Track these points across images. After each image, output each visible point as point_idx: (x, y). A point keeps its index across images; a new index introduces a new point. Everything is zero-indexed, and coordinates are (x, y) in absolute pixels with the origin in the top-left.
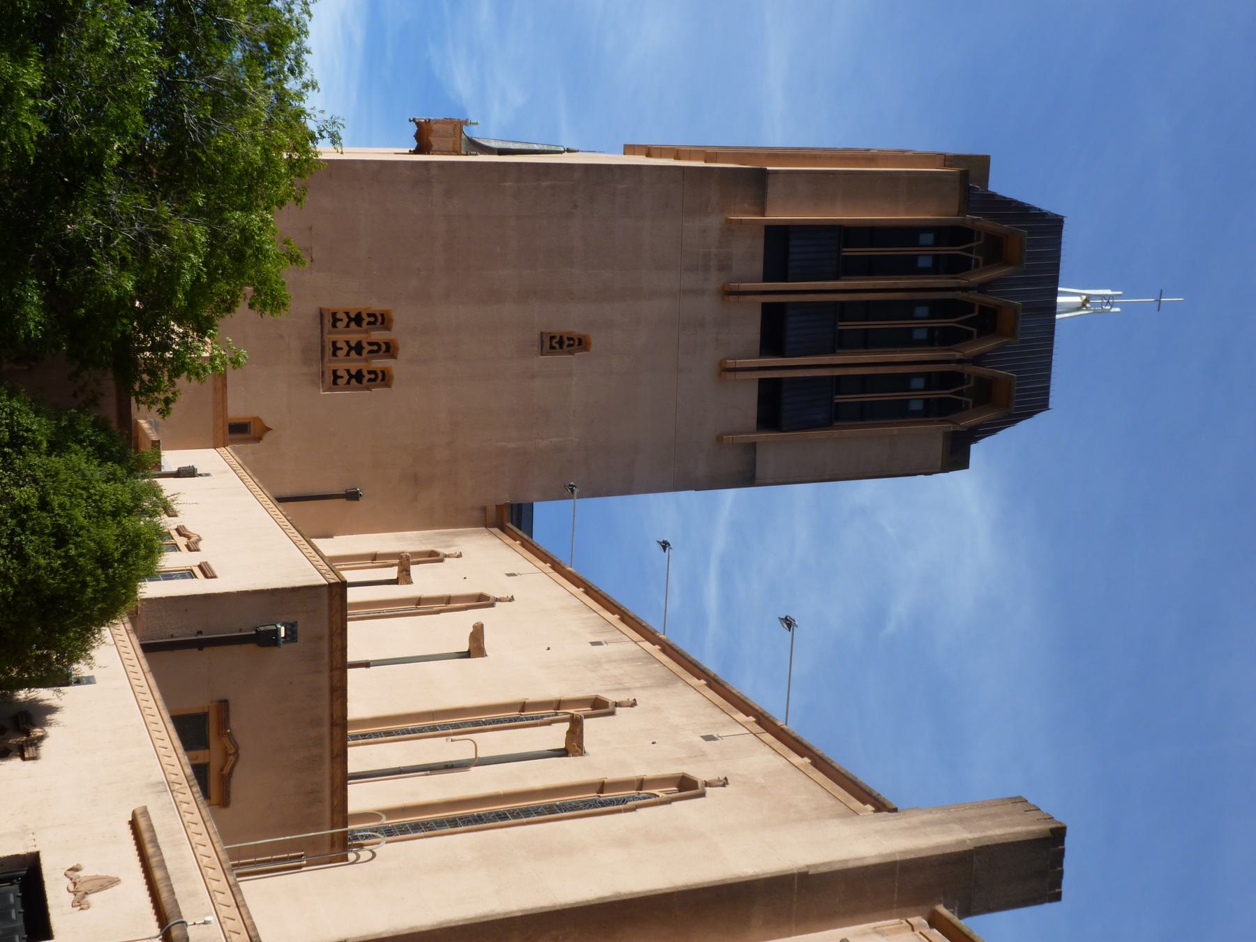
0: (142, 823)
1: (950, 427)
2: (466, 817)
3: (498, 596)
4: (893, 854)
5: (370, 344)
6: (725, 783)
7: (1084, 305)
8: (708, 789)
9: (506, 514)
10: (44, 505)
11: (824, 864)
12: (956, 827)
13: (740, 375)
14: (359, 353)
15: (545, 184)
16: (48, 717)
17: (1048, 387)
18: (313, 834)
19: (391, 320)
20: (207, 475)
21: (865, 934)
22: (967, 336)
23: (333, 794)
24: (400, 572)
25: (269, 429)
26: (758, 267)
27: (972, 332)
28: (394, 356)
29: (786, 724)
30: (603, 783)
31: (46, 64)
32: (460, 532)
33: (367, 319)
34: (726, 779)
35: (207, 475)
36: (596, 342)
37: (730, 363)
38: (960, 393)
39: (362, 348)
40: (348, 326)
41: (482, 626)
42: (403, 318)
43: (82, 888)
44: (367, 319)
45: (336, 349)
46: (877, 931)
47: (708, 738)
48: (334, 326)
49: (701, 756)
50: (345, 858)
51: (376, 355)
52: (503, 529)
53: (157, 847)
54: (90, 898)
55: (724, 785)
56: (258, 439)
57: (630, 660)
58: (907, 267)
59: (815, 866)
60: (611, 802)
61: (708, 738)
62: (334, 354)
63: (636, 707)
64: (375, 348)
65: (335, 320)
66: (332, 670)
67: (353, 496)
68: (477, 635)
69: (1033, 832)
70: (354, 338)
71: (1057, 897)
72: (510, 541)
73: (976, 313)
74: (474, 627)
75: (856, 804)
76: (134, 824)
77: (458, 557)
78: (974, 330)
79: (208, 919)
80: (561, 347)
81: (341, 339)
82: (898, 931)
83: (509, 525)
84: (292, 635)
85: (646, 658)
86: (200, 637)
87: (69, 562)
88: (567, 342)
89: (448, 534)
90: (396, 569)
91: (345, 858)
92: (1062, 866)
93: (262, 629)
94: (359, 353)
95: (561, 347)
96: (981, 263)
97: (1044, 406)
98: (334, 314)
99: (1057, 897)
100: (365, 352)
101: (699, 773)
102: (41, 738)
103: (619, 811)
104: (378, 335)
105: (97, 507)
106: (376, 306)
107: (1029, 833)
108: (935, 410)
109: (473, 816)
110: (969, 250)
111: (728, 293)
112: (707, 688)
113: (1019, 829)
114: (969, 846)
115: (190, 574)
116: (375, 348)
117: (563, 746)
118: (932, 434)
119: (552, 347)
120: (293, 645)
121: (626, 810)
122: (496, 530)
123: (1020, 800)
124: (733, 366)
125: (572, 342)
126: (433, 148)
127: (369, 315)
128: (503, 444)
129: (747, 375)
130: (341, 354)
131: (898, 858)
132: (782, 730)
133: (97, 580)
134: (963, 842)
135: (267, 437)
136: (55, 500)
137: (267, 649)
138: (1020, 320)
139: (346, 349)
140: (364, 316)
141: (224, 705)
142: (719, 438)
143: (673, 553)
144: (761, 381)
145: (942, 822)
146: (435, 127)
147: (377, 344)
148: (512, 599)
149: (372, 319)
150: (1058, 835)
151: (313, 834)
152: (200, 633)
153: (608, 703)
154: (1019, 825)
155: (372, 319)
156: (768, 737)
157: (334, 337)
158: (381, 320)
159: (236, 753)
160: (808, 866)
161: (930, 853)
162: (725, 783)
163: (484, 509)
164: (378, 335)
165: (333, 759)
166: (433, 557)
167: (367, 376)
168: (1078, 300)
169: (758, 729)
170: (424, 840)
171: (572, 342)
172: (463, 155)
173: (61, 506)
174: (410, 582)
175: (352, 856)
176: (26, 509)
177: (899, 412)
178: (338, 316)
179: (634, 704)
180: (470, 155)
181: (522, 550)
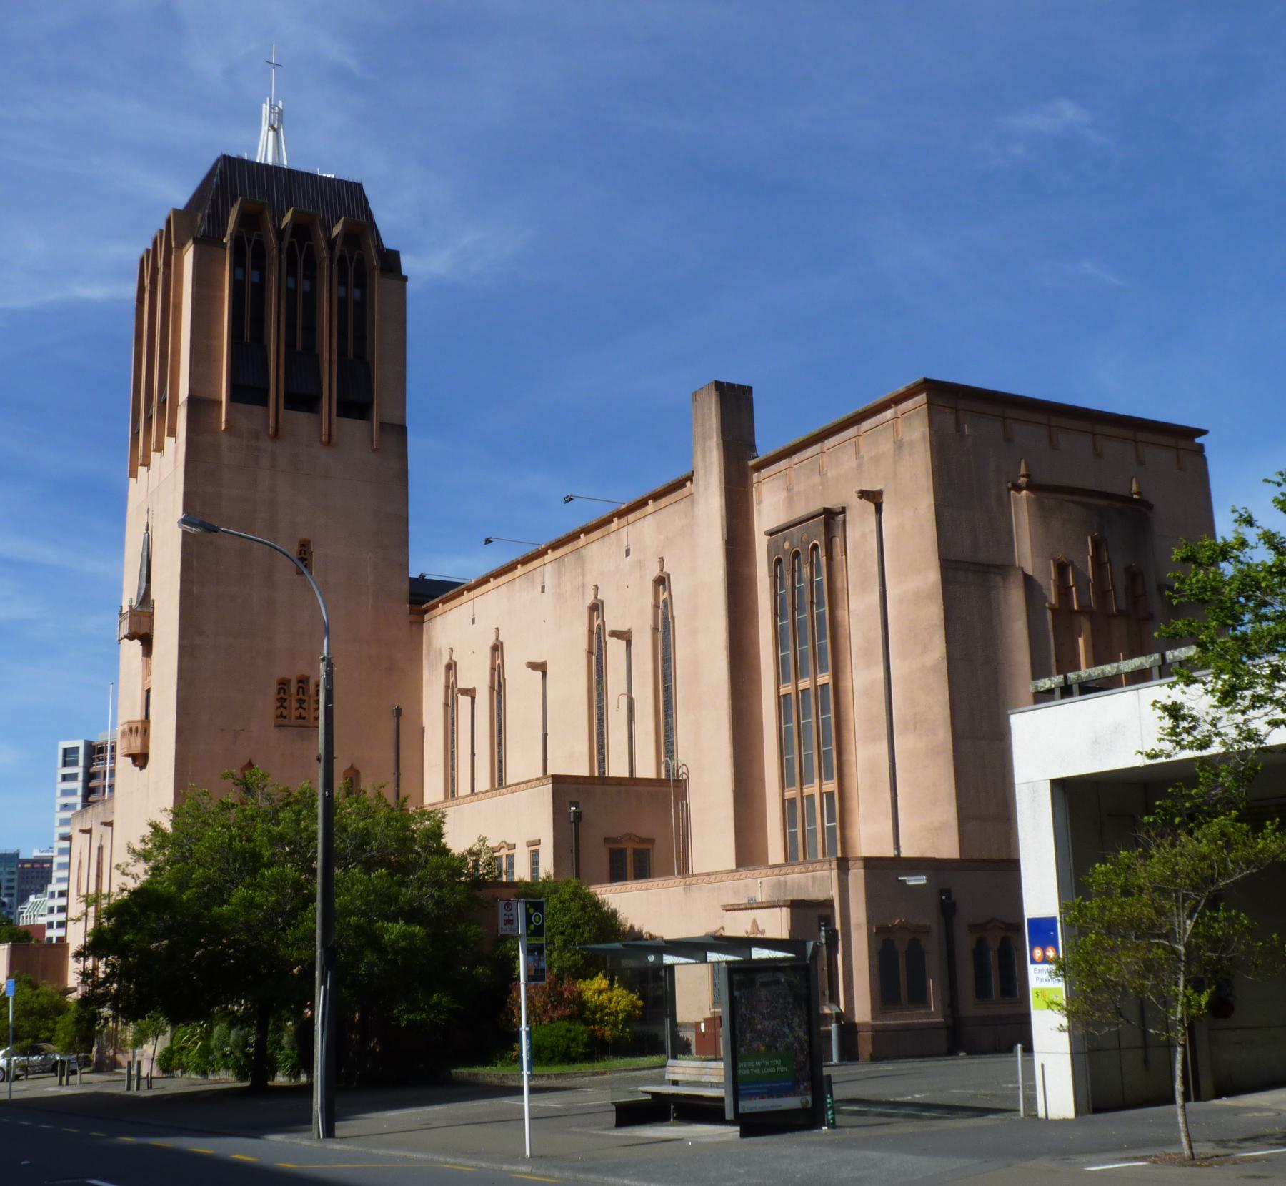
0: (727, 908)
1: (377, 272)
2: (665, 708)
3: (494, 638)
4: (721, 488)
5: (298, 694)
6: (662, 560)
7: (275, 130)
8: (664, 570)
9: (416, 607)
10: (562, 933)
11: (722, 529)
12: (708, 444)
13: (334, 432)
14: (304, 701)
15: (195, 563)
16: (636, 930)
17: (346, 182)
18: (672, 797)
19: (284, 679)
21: (759, 510)
22: (310, 249)
23: (653, 786)
25: (352, 766)
26: (257, 409)
28: (308, 678)
29: (624, 504)
30: (654, 628)
31: (32, 890)
32: (427, 642)
33: (282, 695)
34: (660, 558)
36: (304, 535)
37: (324, 438)
38: (351, 258)
40: (304, 709)
41: (528, 663)
42: (284, 669)
43: (756, 930)
44: (282, 695)
45: (301, 717)
46: (759, 503)
47: (628, 553)
48: (285, 717)
49: (640, 564)
50: (685, 780)
51: (305, 690)
52: (426, 611)
53: (742, 904)
54: (760, 928)
55: (663, 561)
56: (357, 772)
57: (559, 574)
58: (260, 290)
59: (723, 535)
60: (665, 626)
61: (628, 553)
62: (304, 718)
63: (599, 586)
64: (301, 690)
65: (282, 716)
66: (594, 784)
67: (398, 712)
69: (717, 401)
70: (295, 705)
71: (750, 388)
72: (435, 612)
74: (528, 667)
75: (685, 491)
76: (727, 911)
77: (452, 651)
78: (307, 243)
79: (759, 882)
81: (295, 713)
82: (759, 491)
83: (424, 606)
84: (576, 804)
86: (574, 851)
87: (586, 923)
88: (303, 556)
89: (428, 651)
91: (685, 780)
92: (734, 385)
93: (572, 819)
94: (304, 701)
97: (358, 187)
98: (278, 717)
99: (750, 388)
100: (304, 698)
101: (654, 572)
102: (650, 935)
103: (674, 626)
104: (293, 688)
106: (273, 689)
107: (717, 404)
108: (362, 282)
109: (664, 705)
111: (276, 435)
112: (588, 536)
113: (714, 401)
114: (721, 441)
115: (535, 854)
116: (301, 690)
117: (624, 642)
118: (379, 284)
120: (581, 804)
121: (674, 623)
122: (427, 617)
123: (694, 395)
124: (327, 436)
125: (303, 552)
126: (148, 632)
127: (279, 693)
128: (370, 607)
129: (334, 427)
130: (304, 714)
131: (723, 487)
132: (627, 507)
133: (591, 911)
134: (717, 445)
135: (357, 767)
136: (561, 929)
138: (303, 209)
139: (301, 710)
140: (280, 696)
141: (606, 840)
142: (375, 450)
143: (493, 537)
144: (338, 415)
145: (704, 450)
146: (133, 630)
147: (299, 688)
148: (497, 629)
150: (720, 386)
151: (672, 797)
152: (572, 851)
153: (594, 603)
154: (711, 409)
155: (282, 691)
156: (631, 517)
157: (293, 718)
158: (283, 685)
159: (629, 834)
160: (723, 539)
161: (722, 467)
162: (662, 560)
163: (411, 623)
164: (293, 688)
165: (637, 785)
166: (451, 667)
168: (271, 134)
169: (624, 520)
170: (678, 736)
171: (303, 552)
172: (153, 611)
173: (563, 926)
174: (474, 690)
175: (685, 777)
176: (565, 940)
177: (362, 308)
178: (279, 714)
179: (596, 587)
180: (153, 605)
181: (448, 605)
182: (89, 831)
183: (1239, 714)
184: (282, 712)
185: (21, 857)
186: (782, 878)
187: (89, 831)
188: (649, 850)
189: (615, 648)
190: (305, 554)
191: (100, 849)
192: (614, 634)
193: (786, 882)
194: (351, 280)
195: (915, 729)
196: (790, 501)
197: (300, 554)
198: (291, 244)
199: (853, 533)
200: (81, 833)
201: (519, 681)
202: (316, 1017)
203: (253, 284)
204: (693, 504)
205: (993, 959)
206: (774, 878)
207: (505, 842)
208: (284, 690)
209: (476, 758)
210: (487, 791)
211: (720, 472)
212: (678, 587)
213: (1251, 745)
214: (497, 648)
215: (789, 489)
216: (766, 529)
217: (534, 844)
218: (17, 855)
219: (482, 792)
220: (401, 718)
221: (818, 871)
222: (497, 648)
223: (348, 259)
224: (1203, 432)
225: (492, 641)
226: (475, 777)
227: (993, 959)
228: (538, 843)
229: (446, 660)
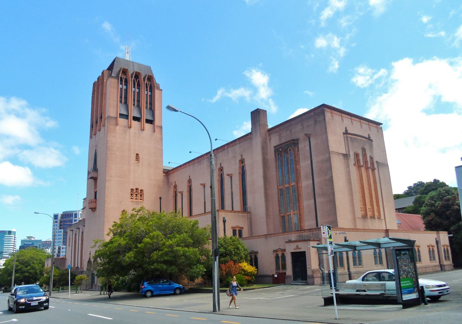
22: (138, 81)
38: (148, 84)
68: (228, 175)
143: (218, 138)
158: (132, 190)
182: (72, 231)
185: (42, 241)
186: (301, 234)
187: (72, 231)
188: (241, 230)
189: (179, 196)
191: (76, 234)
192: (179, 192)
193: (302, 235)
194: (148, 90)
195: (323, 196)
196: (280, 139)
198: (134, 79)
199: (301, 146)
200: (368, 135)
202: (51, 278)
203: (125, 89)
204: (251, 140)
205: (446, 252)
206: (298, 234)
210: (203, 213)
212: (247, 163)
214: (190, 181)
215: (280, 136)
216: (274, 146)
218: (41, 240)
219: (195, 216)
220: (161, 200)
221: (314, 231)
222: (190, 181)
224: (382, 124)
225: (188, 179)
226: (206, 208)
227: (446, 252)
229: (174, 184)
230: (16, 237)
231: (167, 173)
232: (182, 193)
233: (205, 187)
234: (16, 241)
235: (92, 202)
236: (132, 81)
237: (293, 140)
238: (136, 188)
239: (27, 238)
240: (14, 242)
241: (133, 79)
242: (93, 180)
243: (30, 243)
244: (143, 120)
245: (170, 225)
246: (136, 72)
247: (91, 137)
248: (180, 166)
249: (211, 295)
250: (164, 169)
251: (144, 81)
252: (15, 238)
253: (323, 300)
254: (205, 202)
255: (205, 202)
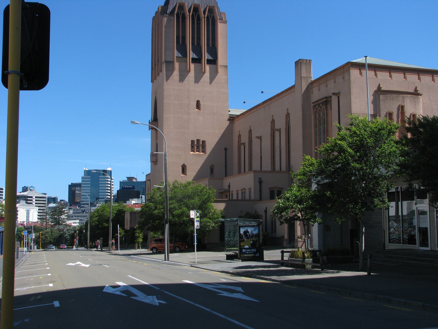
20: (230, 183)
22: (199, 15)
24: (243, 145)
27: (198, 14)
35: (230, 183)
39: (198, 146)
40: (194, 148)
64: (198, 143)
68: (257, 137)
73: (194, 13)
78: (197, 13)
80: (199, 106)
85: (264, 108)
90: (242, 145)
95: (199, 106)
96: (183, 11)
105: (301, 237)
110: (181, 14)
119: (199, 108)
137: (178, 71)
149: (192, 144)
155: (203, 144)
158: (193, 142)
167: (203, 145)
178: (203, 151)
183: (335, 155)
184: (203, 150)
189: (277, 133)
190: (198, 104)
197: (197, 104)
201: (256, 142)
207: (244, 188)
208: (204, 144)
209: (224, 165)
211: (218, 53)
213: (52, 205)
214: (288, 115)
217: (250, 189)
220: (227, 151)
223: (209, 17)
226: (245, 168)
228: (251, 188)
230: (112, 178)
231: (232, 119)
232: (279, 130)
233: (262, 140)
234: (112, 181)
235: (153, 155)
236: (189, 16)
237: (326, 98)
238: (197, 140)
239: (126, 179)
240: (110, 181)
241: (191, 14)
242: (155, 130)
243: (130, 187)
244: (204, 60)
245: (407, 131)
246: (195, 5)
247: (152, 81)
248: (278, 95)
249: (164, 255)
250: (229, 115)
251: (204, 14)
252: (111, 179)
253: (226, 256)
254: (261, 157)
255: (261, 157)
